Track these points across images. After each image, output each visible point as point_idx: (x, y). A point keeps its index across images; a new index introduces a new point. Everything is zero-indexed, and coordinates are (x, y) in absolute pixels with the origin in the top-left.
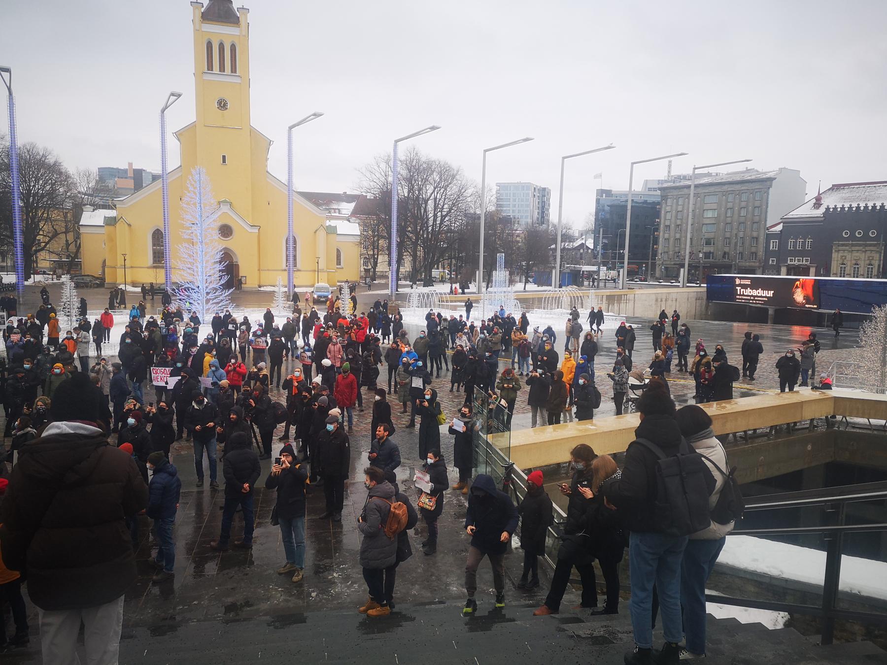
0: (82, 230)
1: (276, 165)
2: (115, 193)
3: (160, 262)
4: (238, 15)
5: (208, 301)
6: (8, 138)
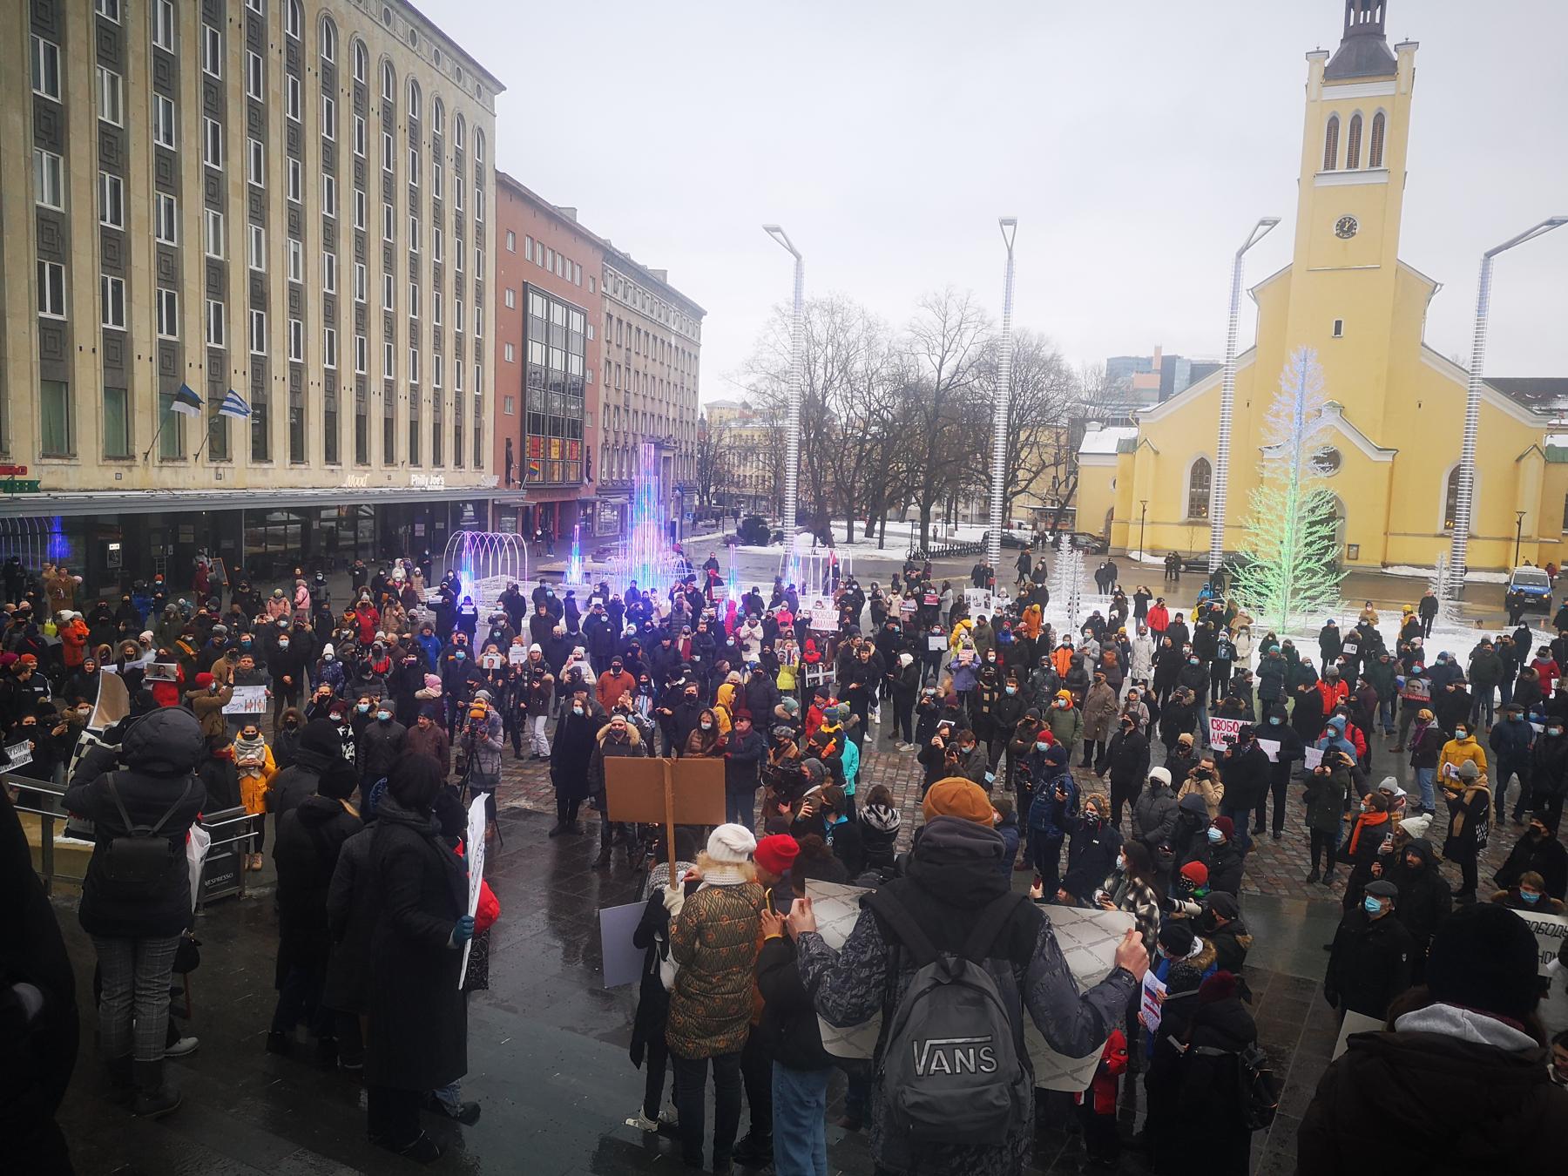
0: (1082, 461)
1: (1446, 327)
2: (1138, 399)
3: (1199, 514)
4: (1396, 56)
5: (1295, 592)
6: (999, 325)
